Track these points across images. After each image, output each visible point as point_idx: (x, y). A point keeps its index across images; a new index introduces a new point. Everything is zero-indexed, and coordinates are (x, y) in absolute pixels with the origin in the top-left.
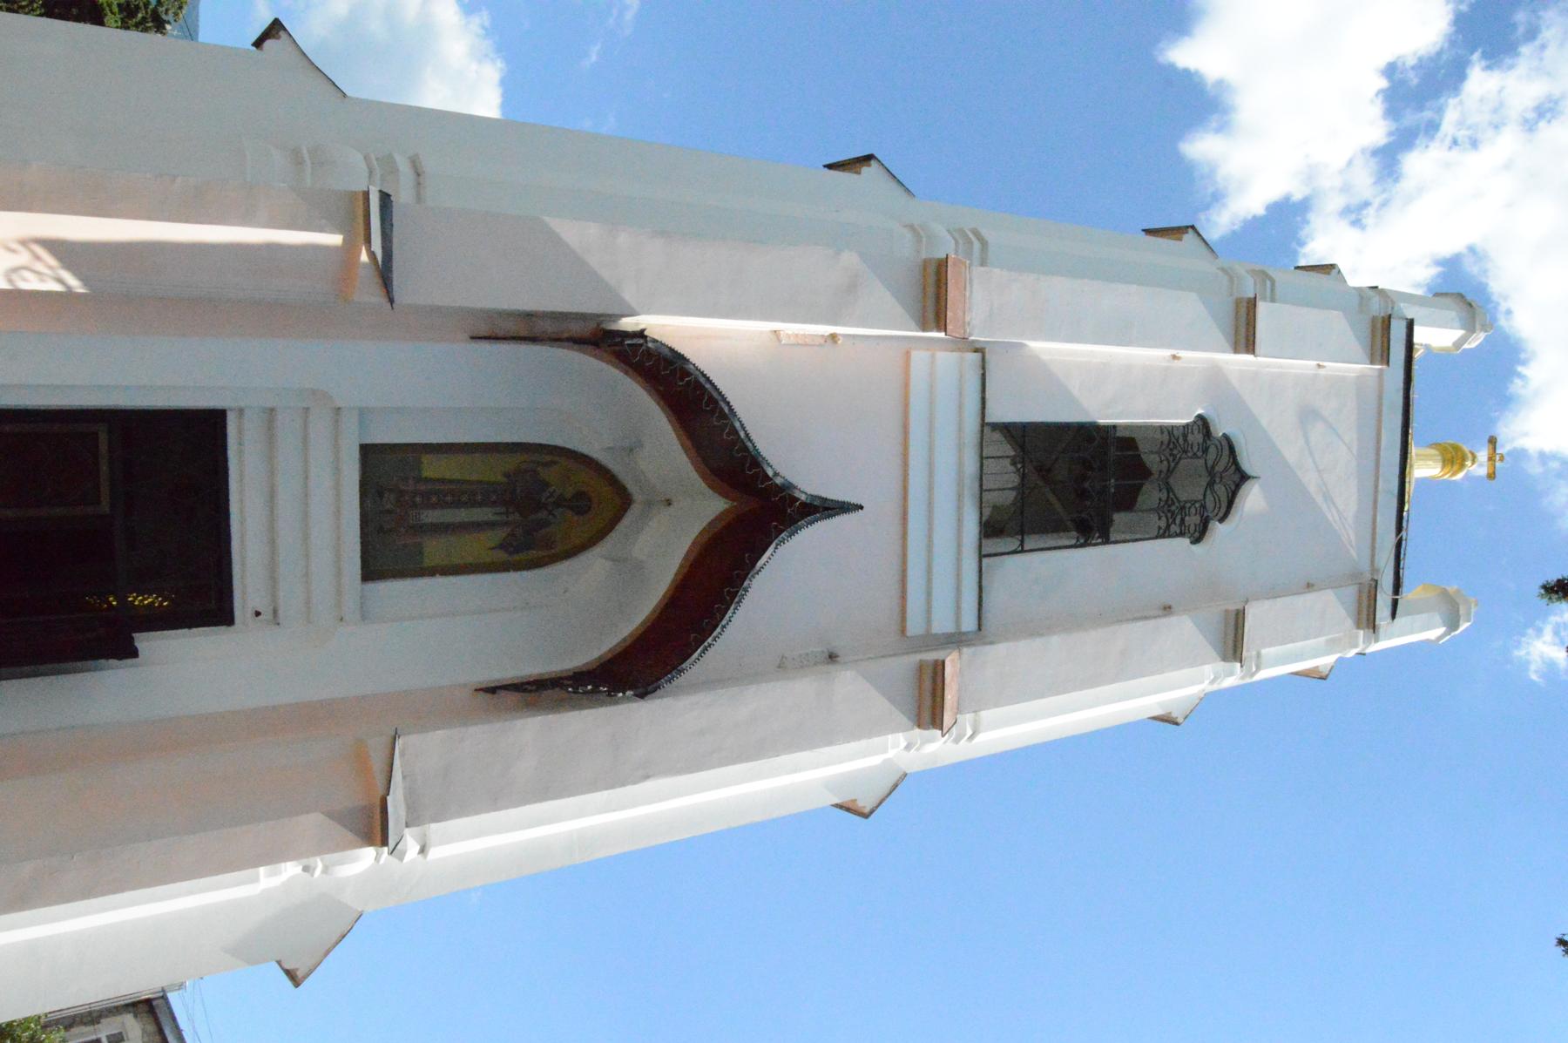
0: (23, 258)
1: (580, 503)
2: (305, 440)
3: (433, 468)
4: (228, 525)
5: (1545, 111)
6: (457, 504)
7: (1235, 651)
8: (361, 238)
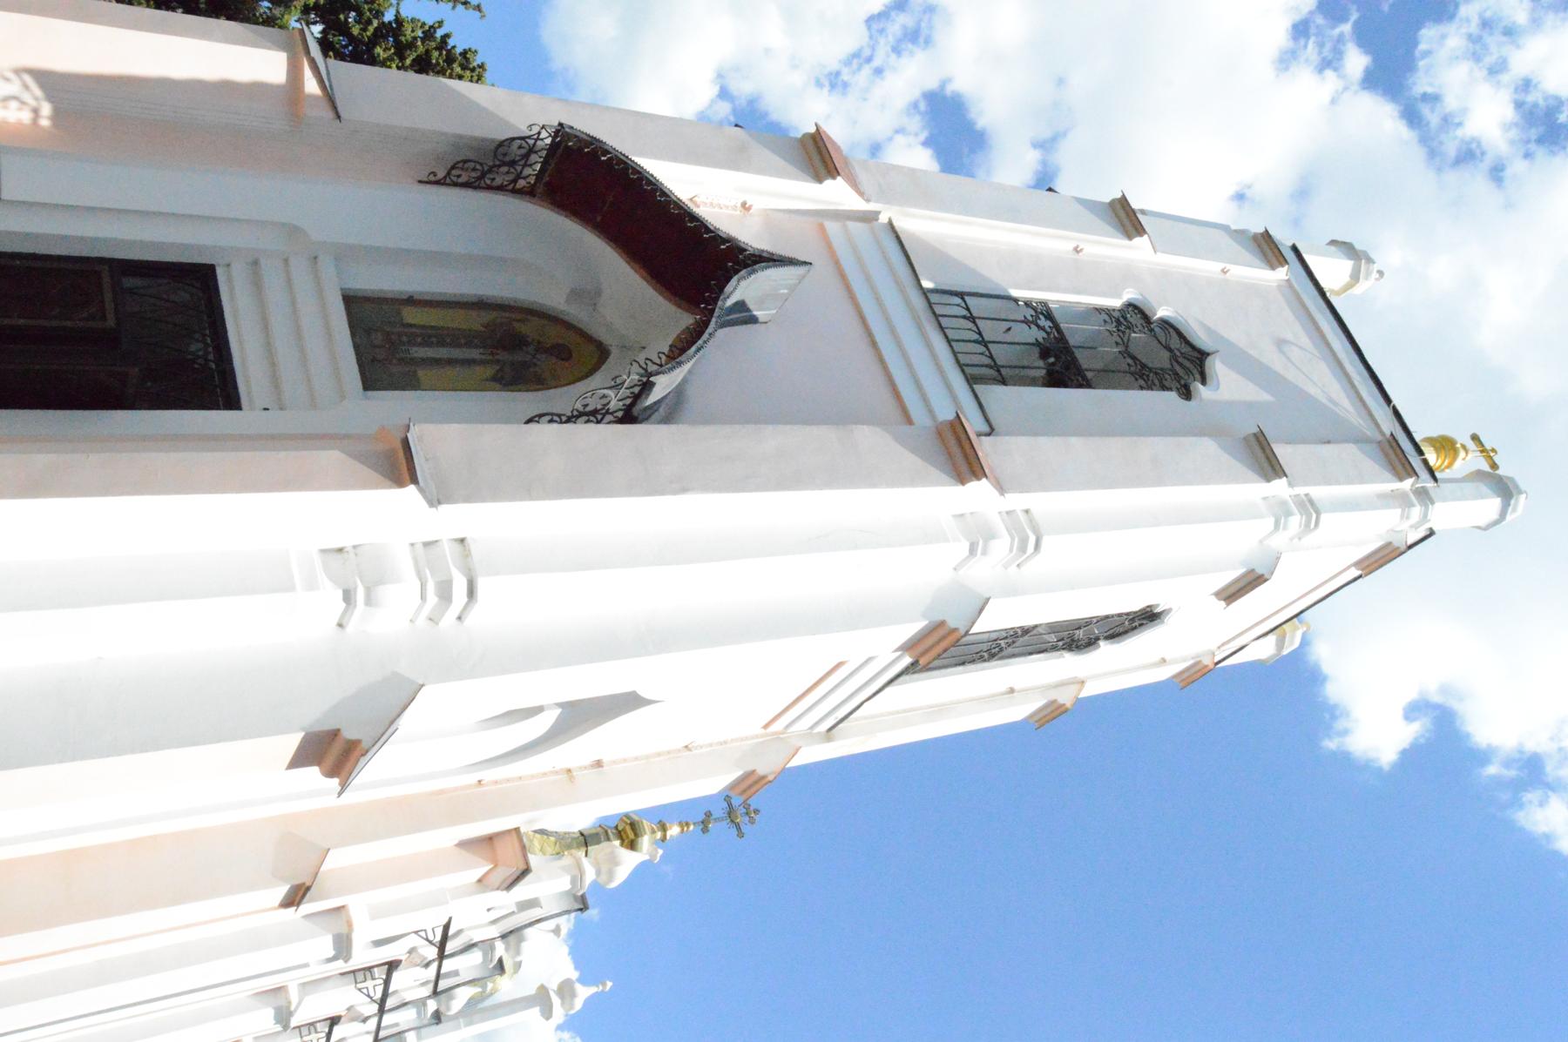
0: (14, 88)
1: (562, 353)
2: (289, 281)
3: (412, 316)
4: (229, 349)
5: (1347, 248)
6: (442, 343)
7: (826, 166)
8: (300, 48)
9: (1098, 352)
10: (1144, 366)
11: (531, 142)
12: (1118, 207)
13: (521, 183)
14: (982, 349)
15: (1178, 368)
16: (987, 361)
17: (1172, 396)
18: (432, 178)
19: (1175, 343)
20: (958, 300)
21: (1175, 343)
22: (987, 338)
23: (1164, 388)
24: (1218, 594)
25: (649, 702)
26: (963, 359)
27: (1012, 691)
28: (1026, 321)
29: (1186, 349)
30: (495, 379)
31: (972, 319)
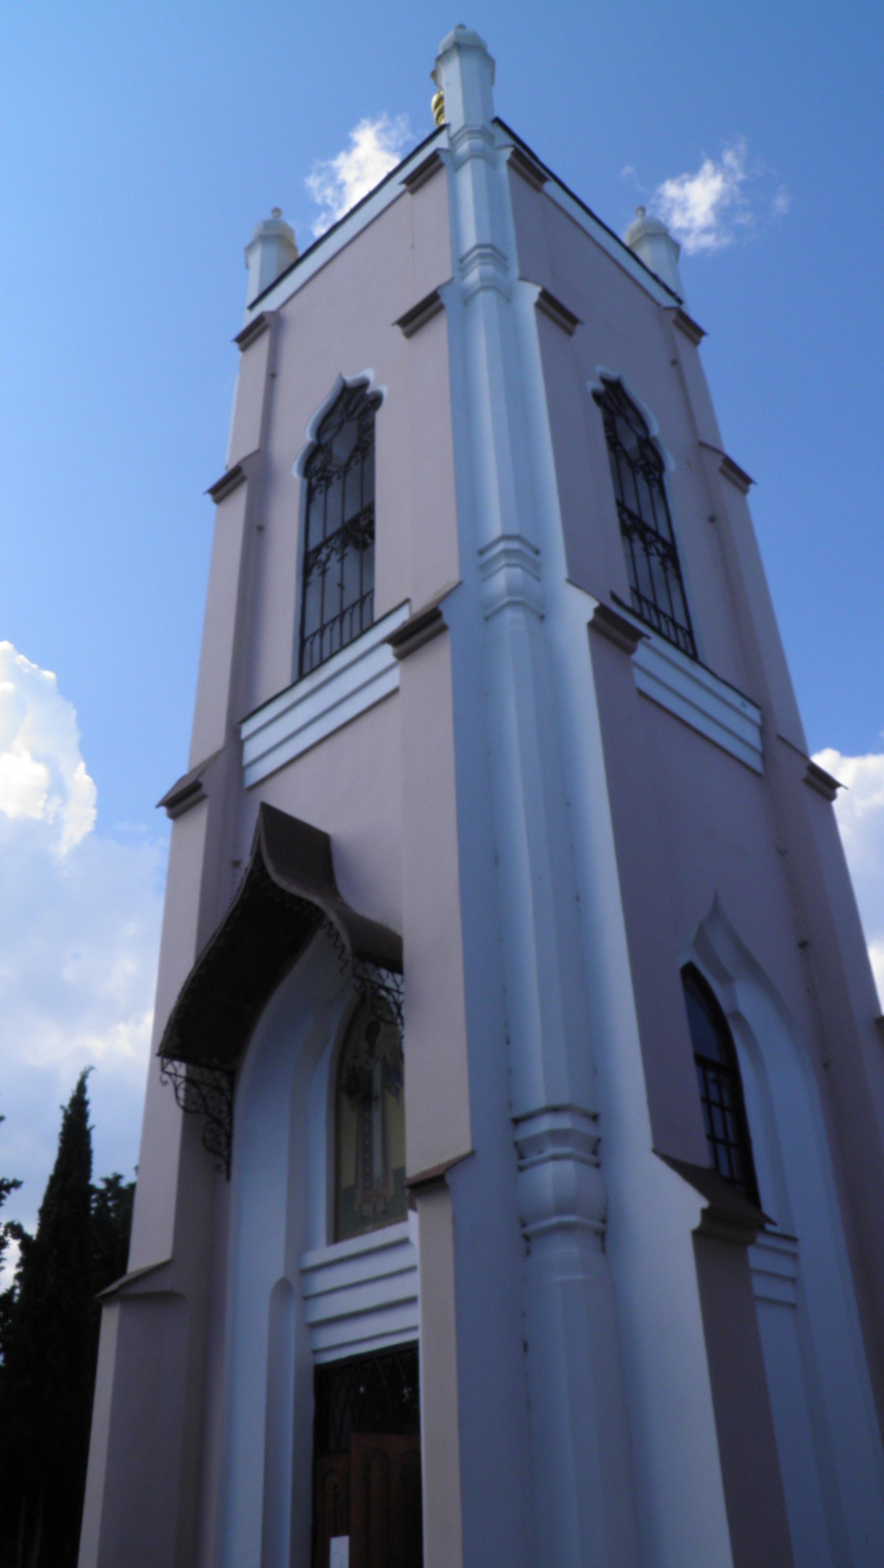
9: (337, 509)
11: (205, 1090)
12: (414, 185)
13: (224, 1084)
14: (327, 632)
15: (356, 414)
16: (337, 625)
18: (224, 1168)
19: (336, 419)
20: (308, 645)
21: (336, 419)
24: (570, 333)
26: (336, 646)
27: (712, 519)
28: (324, 573)
29: (341, 406)
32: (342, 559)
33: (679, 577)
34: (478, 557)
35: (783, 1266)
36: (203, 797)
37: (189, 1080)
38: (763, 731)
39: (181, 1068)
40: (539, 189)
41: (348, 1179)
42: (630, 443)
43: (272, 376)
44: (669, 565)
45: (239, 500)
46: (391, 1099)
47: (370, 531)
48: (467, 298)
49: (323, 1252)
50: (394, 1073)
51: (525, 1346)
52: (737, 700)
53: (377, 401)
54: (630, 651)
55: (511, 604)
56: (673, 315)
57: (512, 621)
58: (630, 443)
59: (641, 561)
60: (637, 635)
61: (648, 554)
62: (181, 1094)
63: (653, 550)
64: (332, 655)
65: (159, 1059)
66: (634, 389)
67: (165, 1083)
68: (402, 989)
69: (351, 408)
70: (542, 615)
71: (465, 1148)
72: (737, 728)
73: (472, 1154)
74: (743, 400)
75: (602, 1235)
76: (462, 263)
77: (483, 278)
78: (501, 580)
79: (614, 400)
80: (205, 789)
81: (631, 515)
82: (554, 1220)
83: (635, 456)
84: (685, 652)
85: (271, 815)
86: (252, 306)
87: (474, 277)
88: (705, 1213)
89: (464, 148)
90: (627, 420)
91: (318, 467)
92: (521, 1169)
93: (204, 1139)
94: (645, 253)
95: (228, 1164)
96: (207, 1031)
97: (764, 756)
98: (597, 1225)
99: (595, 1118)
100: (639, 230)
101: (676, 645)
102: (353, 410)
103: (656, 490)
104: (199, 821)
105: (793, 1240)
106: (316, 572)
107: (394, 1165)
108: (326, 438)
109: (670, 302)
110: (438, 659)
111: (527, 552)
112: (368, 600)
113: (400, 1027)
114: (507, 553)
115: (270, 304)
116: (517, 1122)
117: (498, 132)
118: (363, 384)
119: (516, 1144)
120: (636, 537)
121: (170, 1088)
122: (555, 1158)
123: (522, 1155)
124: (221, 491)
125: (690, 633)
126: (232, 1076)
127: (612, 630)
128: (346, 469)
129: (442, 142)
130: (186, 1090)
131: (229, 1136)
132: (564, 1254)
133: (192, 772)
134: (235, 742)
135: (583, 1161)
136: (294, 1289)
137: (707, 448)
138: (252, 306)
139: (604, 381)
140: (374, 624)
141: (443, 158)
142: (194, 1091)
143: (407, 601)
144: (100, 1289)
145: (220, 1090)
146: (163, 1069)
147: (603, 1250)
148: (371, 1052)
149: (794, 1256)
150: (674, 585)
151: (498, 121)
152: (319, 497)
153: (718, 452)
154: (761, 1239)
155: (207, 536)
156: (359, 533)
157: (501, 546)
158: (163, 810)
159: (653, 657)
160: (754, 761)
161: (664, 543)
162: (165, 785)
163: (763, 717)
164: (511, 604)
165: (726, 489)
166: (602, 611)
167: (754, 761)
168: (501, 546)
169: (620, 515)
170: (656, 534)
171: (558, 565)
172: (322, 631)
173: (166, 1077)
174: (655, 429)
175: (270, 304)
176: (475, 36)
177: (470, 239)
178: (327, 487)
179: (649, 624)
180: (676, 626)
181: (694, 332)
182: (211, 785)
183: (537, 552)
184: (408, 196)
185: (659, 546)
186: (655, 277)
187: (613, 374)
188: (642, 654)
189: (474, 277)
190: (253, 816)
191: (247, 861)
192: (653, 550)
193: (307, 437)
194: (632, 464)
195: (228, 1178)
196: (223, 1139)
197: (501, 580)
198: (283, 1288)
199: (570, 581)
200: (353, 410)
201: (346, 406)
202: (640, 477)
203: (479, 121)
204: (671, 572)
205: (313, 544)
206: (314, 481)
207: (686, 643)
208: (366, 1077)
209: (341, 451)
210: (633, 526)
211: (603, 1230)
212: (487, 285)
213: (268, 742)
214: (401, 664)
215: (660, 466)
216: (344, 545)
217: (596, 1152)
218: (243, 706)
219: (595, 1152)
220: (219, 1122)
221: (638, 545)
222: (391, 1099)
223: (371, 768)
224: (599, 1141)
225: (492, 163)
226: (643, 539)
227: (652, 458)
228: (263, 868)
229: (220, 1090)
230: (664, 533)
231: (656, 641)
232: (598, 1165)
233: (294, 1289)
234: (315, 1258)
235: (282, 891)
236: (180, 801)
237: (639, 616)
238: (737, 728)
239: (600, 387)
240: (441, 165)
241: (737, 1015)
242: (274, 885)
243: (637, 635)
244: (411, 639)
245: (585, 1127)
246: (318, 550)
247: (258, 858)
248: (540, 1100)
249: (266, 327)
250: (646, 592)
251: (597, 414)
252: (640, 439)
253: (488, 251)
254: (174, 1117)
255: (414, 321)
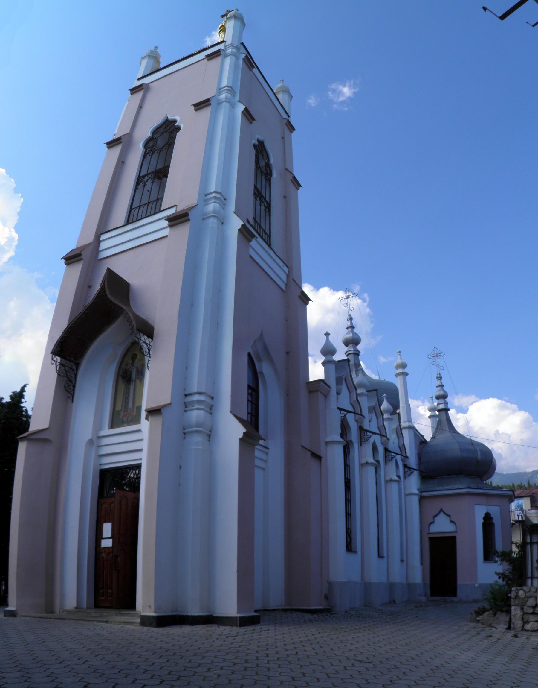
9: (155, 164)
10: (167, 144)
11: (67, 368)
13: (74, 367)
14: (142, 208)
15: (169, 131)
17: (178, 134)
18: (71, 398)
19: (161, 130)
20: (133, 211)
21: (161, 130)
22: (156, 198)
23: (175, 137)
24: (251, 123)
25: (23, 390)
26: (153, 212)
27: (285, 197)
28: (144, 186)
29: (164, 126)
30: (141, 381)
31: (140, 206)
32: (152, 183)
33: (270, 215)
34: (205, 197)
35: (263, 456)
36: (82, 259)
37: (61, 364)
38: (288, 276)
39: (59, 359)
40: (251, 70)
41: (119, 407)
42: (262, 164)
43: (140, 107)
44: (267, 211)
45: (117, 150)
46: (138, 382)
47: (166, 176)
48: (219, 103)
49: (106, 431)
50: (141, 374)
51: (180, 467)
52: (281, 264)
53: (178, 129)
54: (250, 241)
55: (213, 216)
56: (286, 121)
57: (213, 222)
58: (262, 164)
59: (258, 207)
60: (253, 236)
61: (261, 205)
62: (58, 368)
63: (263, 205)
64: (142, 219)
65: (51, 355)
66: (268, 146)
67: (52, 364)
68: (151, 344)
69: (168, 128)
70: (222, 221)
71: (168, 402)
72: (279, 273)
73: (171, 403)
74: (304, 157)
75: (209, 436)
76: (220, 90)
77: (226, 98)
78: (212, 207)
79: (260, 149)
80: (83, 257)
81: (258, 190)
82: (195, 429)
83: (263, 169)
84: (267, 243)
85: (110, 273)
86: (139, 79)
87: (223, 96)
88: (244, 433)
89: (229, 51)
90: (263, 156)
91: (150, 145)
92: (185, 411)
93: (65, 386)
94: (280, 96)
95: (73, 397)
96: (70, 348)
97: (286, 285)
98: (209, 432)
99: (212, 398)
100: (280, 88)
101: (264, 240)
102: (168, 130)
103: (268, 183)
104: (77, 268)
105: (268, 448)
106: (141, 184)
107: (137, 405)
108: (156, 136)
109: (285, 116)
110: (184, 230)
111: (222, 199)
112: (159, 201)
113: (147, 358)
114: (215, 198)
115: (146, 81)
116: (186, 395)
117: (242, 47)
118: (175, 121)
119: (185, 403)
120: (258, 199)
121: (54, 366)
122: (198, 409)
123: (187, 407)
124: (111, 144)
125: (270, 236)
126: (78, 365)
127: (245, 233)
128: (161, 150)
129: (222, 47)
130: (60, 368)
131: (74, 387)
132: (197, 440)
133: (77, 249)
134: (97, 241)
135: (207, 411)
136: (95, 442)
137: (288, 171)
138: (139, 79)
139: (258, 141)
140: (160, 211)
141: (222, 52)
142: (63, 368)
143: (176, 206)
144: (19, 435)
145: (73, 370)
146: (52, 359)
147: (209, 441)
148: (133, 364)
149: (267, 453)
150: (267, 217)
151: (243, 44)
152: (148, 157)
153: (292, 174)
154: (257, 447)
155: (103, 160)
156: (161, 174)
157: (214, 195)
158: (63, 261)
159: (257, 244)
160: (283, 286)
161: (267, 202)
162: (65, 252)
163: (289, 271)
164: (213, 216)
165: (292, 187)
166: (244, 226)
167: (283, 286)
168: (214, 195)
169: (254, 190)
170: (265, 199)
171: (232, 207)
172: (139, 207)
173: (53, 362)
174: (272, 161)
175: (146, 81)
176: (241, 15)
177: (225, 83)
178: (152, 155)
179: (256, 231)
180: (266, 233)
181: (292, 128)
182: (86, 255)
183: (225, 199)
184: (206, 60)
185: (265, 203)
186: (282, 106)
187: (262, 139)
188: (253, 243)
189: (223, 96)
190: (103, 272)
191: (97, 287)
192: (263, 205)
193: (149, 134)
194: (261, 172)
195: (72, 401)
196: (72, 388)
197: (212, 207)
198: (91, 442)
199: (234, 213)
200: (168, 130)
201: (166, 127)
202: (263, 177)
203: (236, 44)
204: (267, 214)
205: (142, 174)
206: (148, 151)
207: (268, 241)
208: (129, 373)
209: (161, 142)
210: (258, 194)
211: (210, 434)
212: (227, 101)
213: (110, 244)
214: (169, 228)
215: (271, 174)
216: (154, 178)
217: (211, 409)
218: (103, 228)
219: (211, 409)
220: (71, 381)
221: (258, 202)
222: (138, 382)
223: (150, 261)
224: (213, 405)
225: (237, 58)
226: (260, 200)
227: (269, 171)
228: (105, 292)
229: (73, 370)
230: (268, 199)
231: (260, 240)
232: (211, 414)
233: (95, 442)
234: (103, 433)
235: (111, 302)
236: (71, 259)
237: (254, 228)
238: (279, 273)
239: (257, 143)
240: (220, 55)
241: (262, 373)
242: (108, 299)
243: (253, 236)
244: (176, 220)
245: (209, 400)
246: (144, 177)
247: (103, 287)
248: (195, 390)
249: (143, 89)
250: (258, 219)
251: (254, 152)
252: (266, 163)
253: (230, 89)
254: (54, 376)
255: (199, 106)
